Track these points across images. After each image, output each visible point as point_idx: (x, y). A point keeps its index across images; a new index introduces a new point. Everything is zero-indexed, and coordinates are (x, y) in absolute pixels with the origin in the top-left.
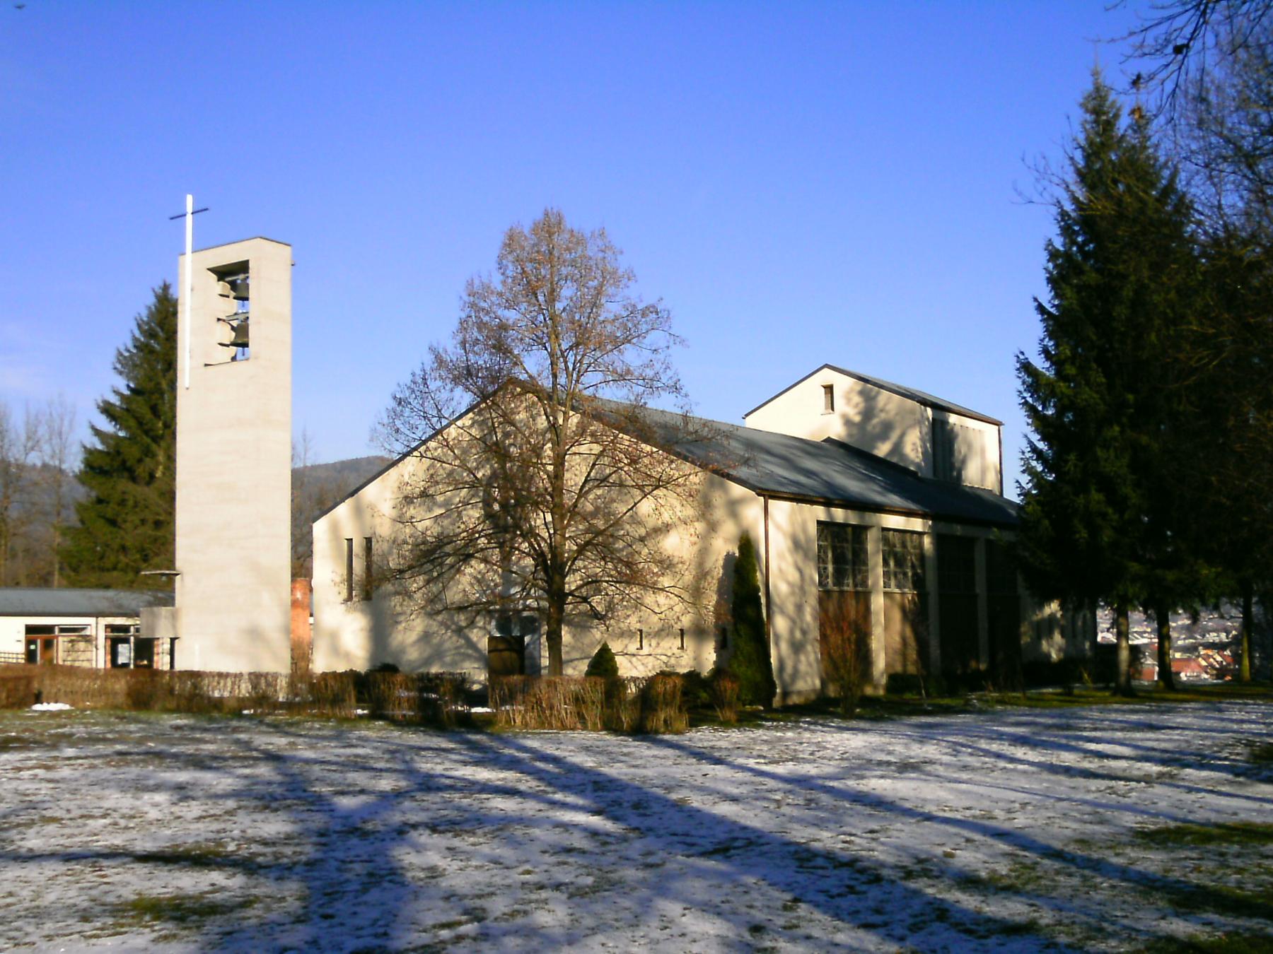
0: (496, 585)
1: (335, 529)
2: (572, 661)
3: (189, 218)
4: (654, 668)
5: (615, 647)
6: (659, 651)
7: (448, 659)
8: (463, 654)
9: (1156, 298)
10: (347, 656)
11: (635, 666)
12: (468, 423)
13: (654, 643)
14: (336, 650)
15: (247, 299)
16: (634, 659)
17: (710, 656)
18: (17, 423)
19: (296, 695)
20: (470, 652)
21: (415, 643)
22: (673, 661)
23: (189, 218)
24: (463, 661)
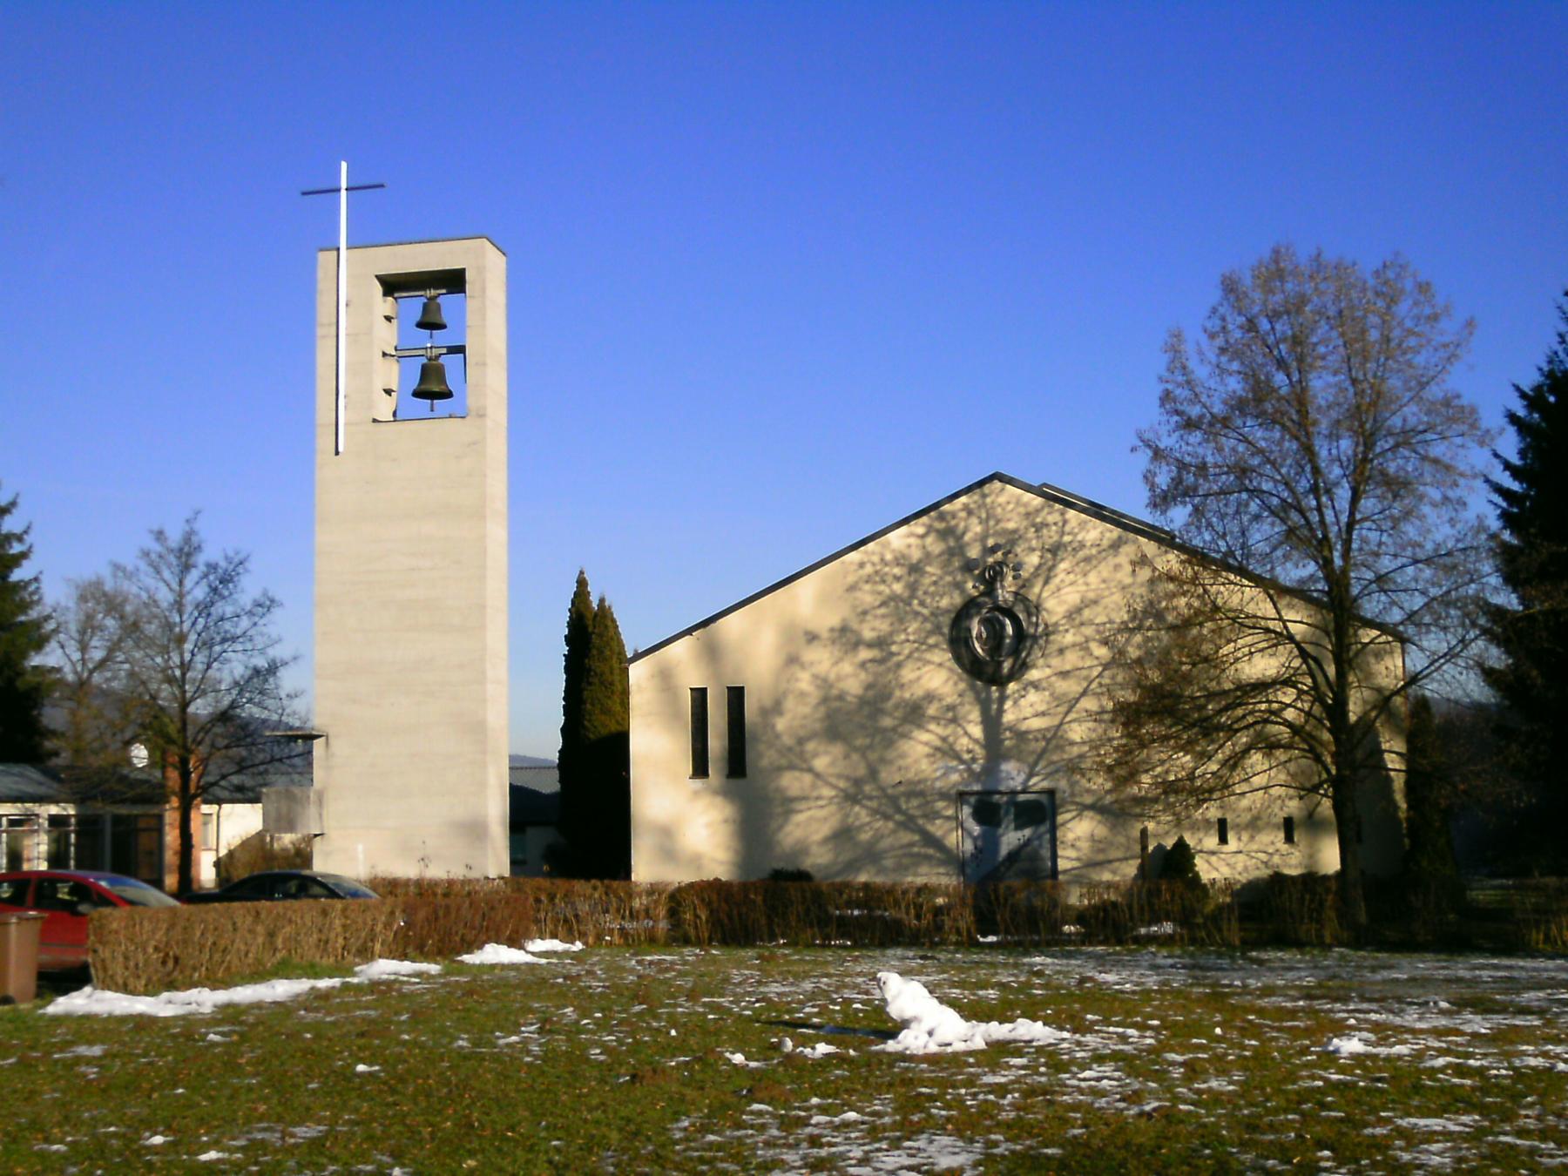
0: (974, 760)
1: (665, 677)
2: (1110, 862)
3: (343, 193)
4: (1246, 868)
5: (1190, 840)
6: (1255, 847)
7: (889, 863)
8: (918, 855)
9: (1101, 781)
10: (696, 860)
11: (1223, 864)
12: (921, 530)
13: (1245, 837)
14: (668, 851)
15: (484, 364)
16: (1213, 859)
17: (1330, 857)
18: (55, 576)
19: (1152, 1153)
20: (931, 851)
21: (826, 840)
22: (1276, 859)
23: (343, 193)
24: (917, 865)
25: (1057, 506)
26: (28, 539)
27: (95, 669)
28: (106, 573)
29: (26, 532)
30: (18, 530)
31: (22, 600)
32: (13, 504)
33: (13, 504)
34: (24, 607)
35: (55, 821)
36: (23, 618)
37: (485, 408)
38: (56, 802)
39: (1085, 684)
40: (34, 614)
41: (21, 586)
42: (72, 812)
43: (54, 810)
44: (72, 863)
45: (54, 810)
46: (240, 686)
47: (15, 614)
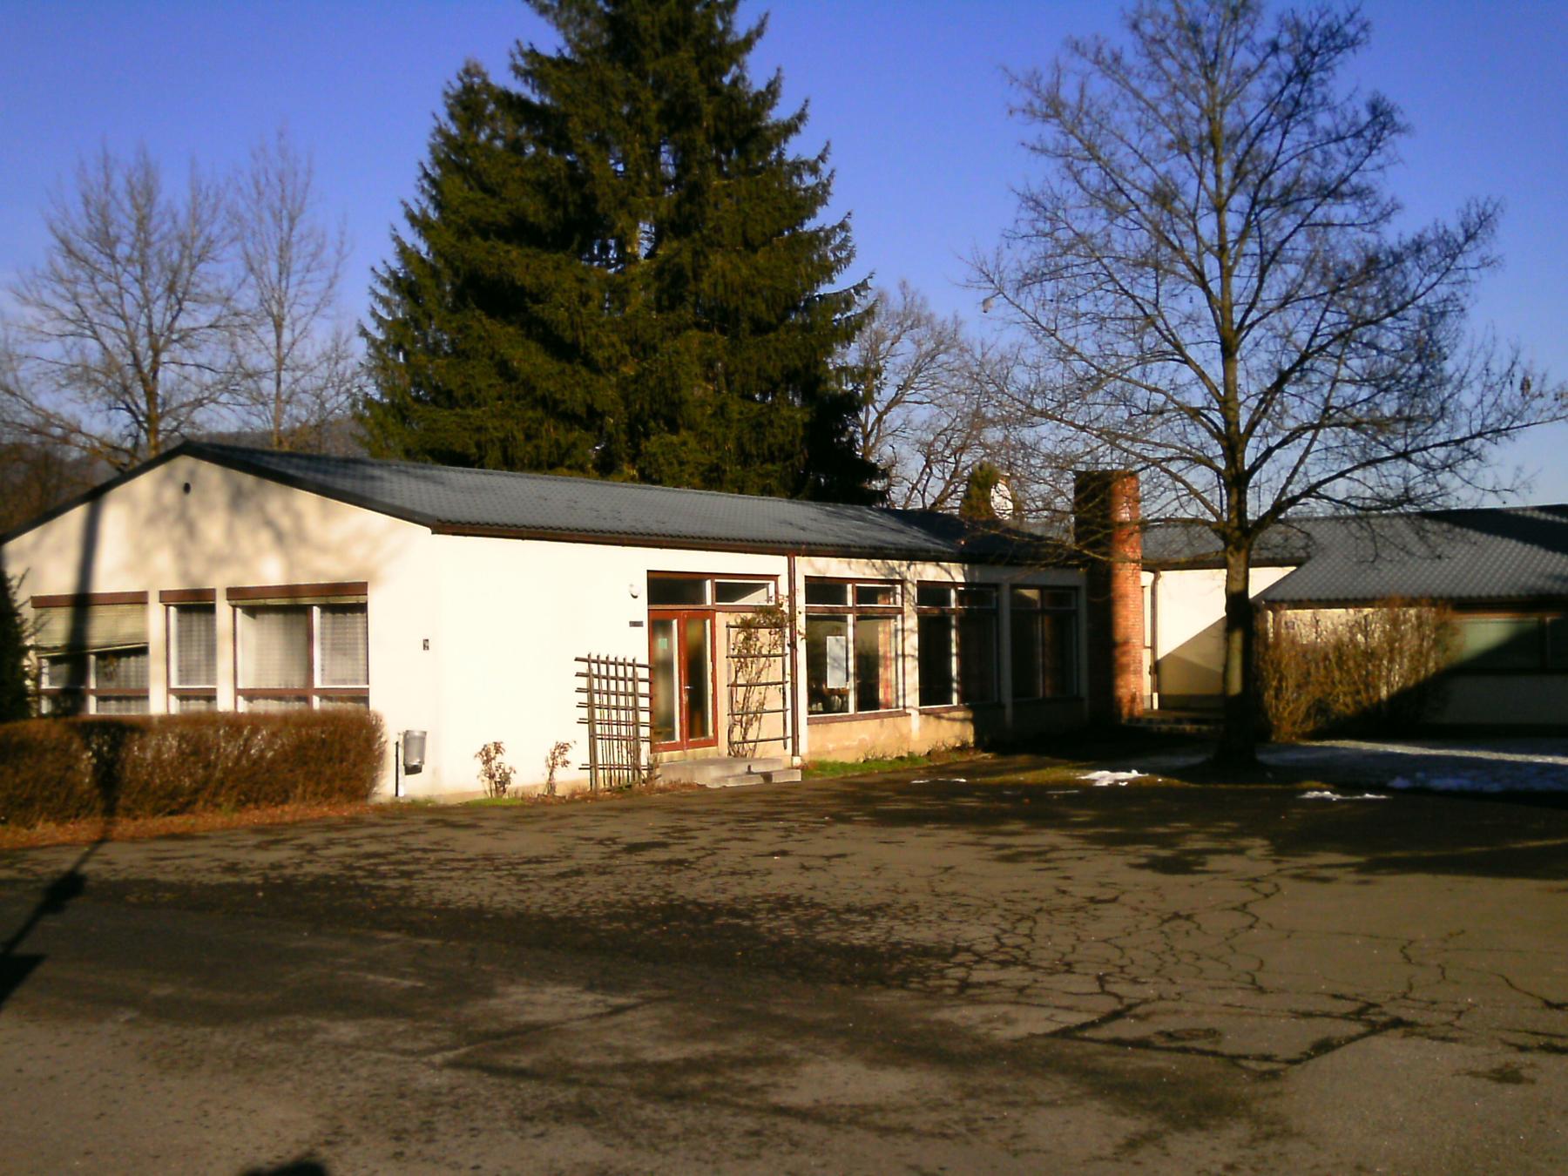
25: (286, 448)
26: (825, 169)
27: (888, 408)
28: (391, 735)
29: (822, 158)
30: (810, 155)
31: (823, 258)
32: (801, 117)
33: (801, 117)
34: (827, 271)
35: (931, 593)
36: (825, 289)
37: (147, 691)
38: (936, 558)
39: (269, 320)
40: (841, 282)
41: (818, 239)
42: (960, 579)
43: (930, 572)
44: (955, 698)
45: (930, 572)
46: (1157, 686)
47: (814, 282)
